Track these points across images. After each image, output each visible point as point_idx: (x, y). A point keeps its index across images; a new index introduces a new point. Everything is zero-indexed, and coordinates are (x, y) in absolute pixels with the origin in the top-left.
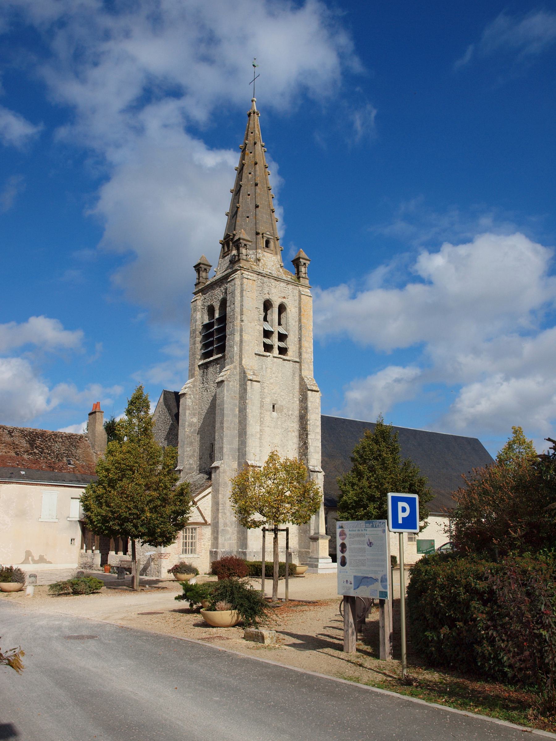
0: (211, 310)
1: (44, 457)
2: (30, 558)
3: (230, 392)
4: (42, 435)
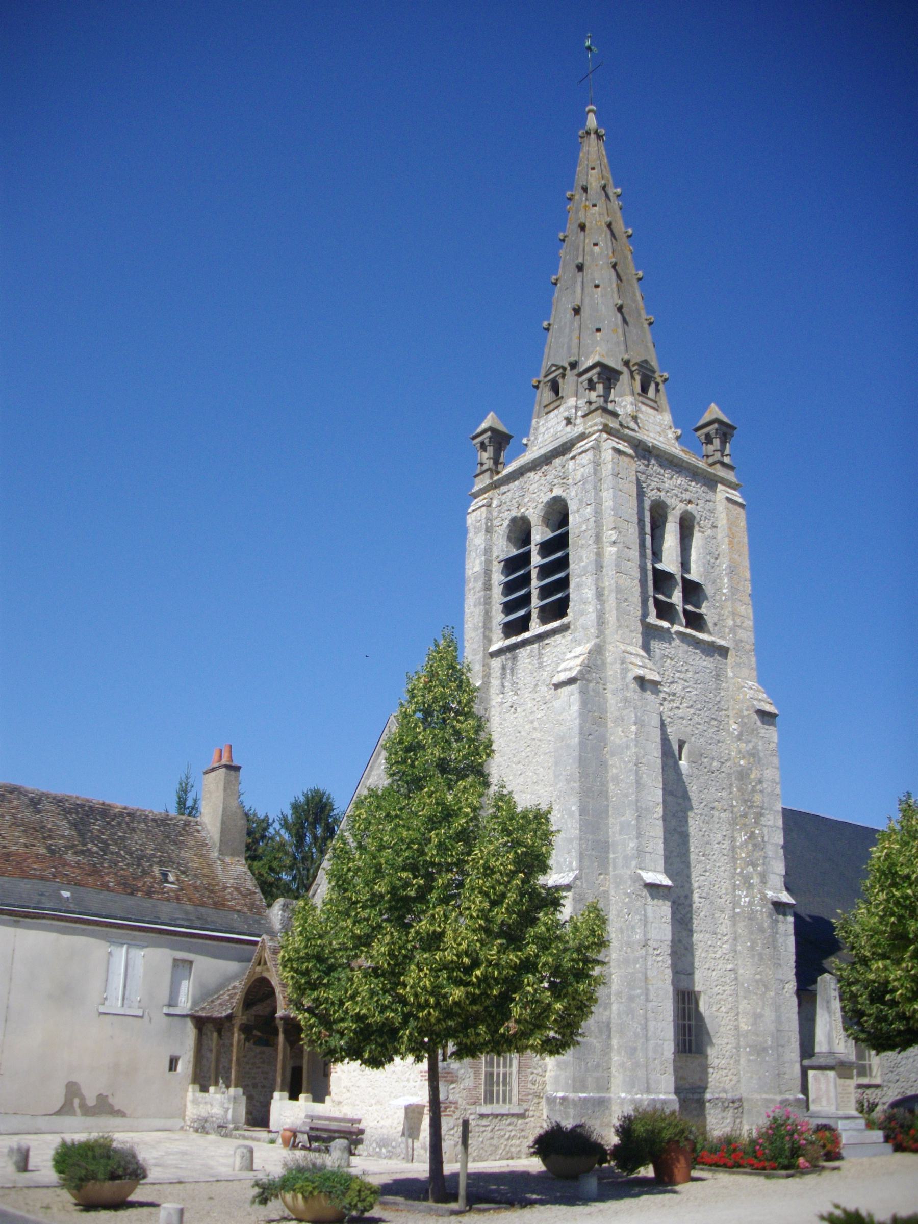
1: (111, 861)
2: (76, 1101)
4: (104, 812)
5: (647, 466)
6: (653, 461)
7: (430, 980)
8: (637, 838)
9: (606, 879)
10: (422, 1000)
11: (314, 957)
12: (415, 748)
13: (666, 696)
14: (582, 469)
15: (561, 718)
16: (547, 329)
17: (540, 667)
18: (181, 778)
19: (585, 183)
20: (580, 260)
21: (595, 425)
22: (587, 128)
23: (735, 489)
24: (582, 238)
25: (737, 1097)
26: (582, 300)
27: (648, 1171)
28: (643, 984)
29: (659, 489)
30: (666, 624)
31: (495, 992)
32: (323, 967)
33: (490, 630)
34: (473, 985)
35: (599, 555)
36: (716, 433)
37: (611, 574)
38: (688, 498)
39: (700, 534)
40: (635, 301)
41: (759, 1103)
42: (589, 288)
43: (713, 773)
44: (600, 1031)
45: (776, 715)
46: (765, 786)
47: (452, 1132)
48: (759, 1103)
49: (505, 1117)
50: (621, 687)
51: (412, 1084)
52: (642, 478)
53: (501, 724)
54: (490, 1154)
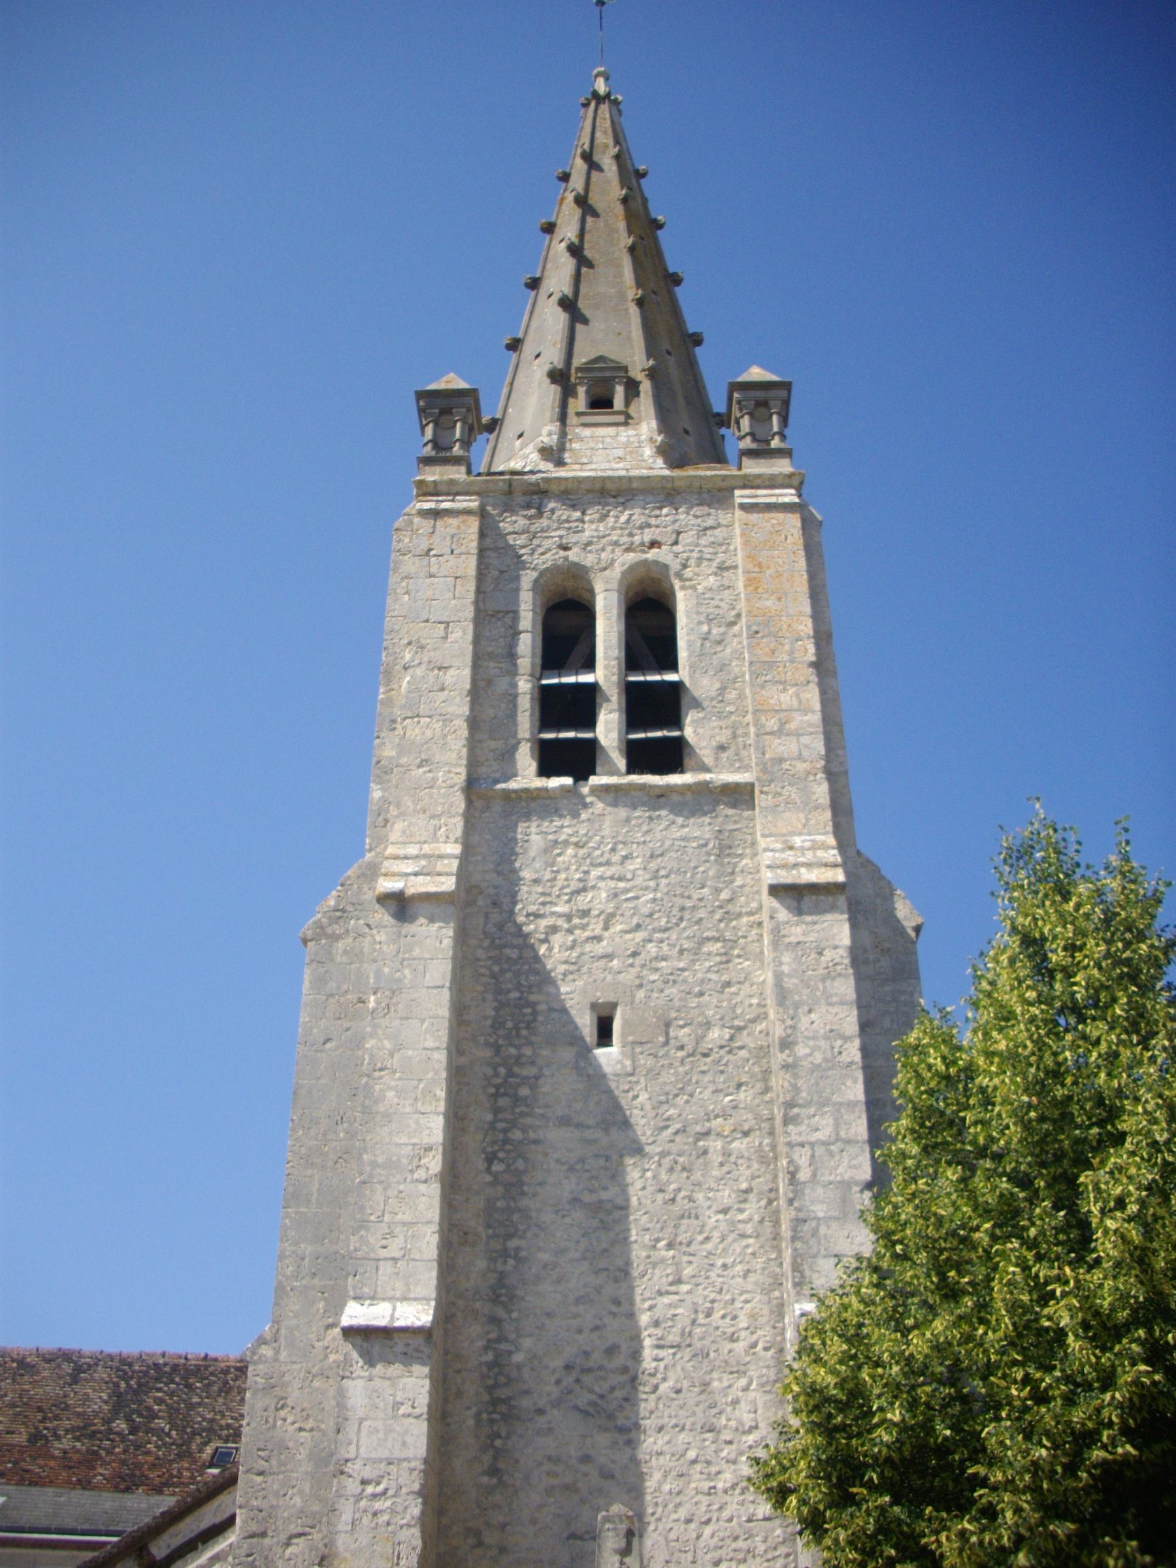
3: (332, 985)
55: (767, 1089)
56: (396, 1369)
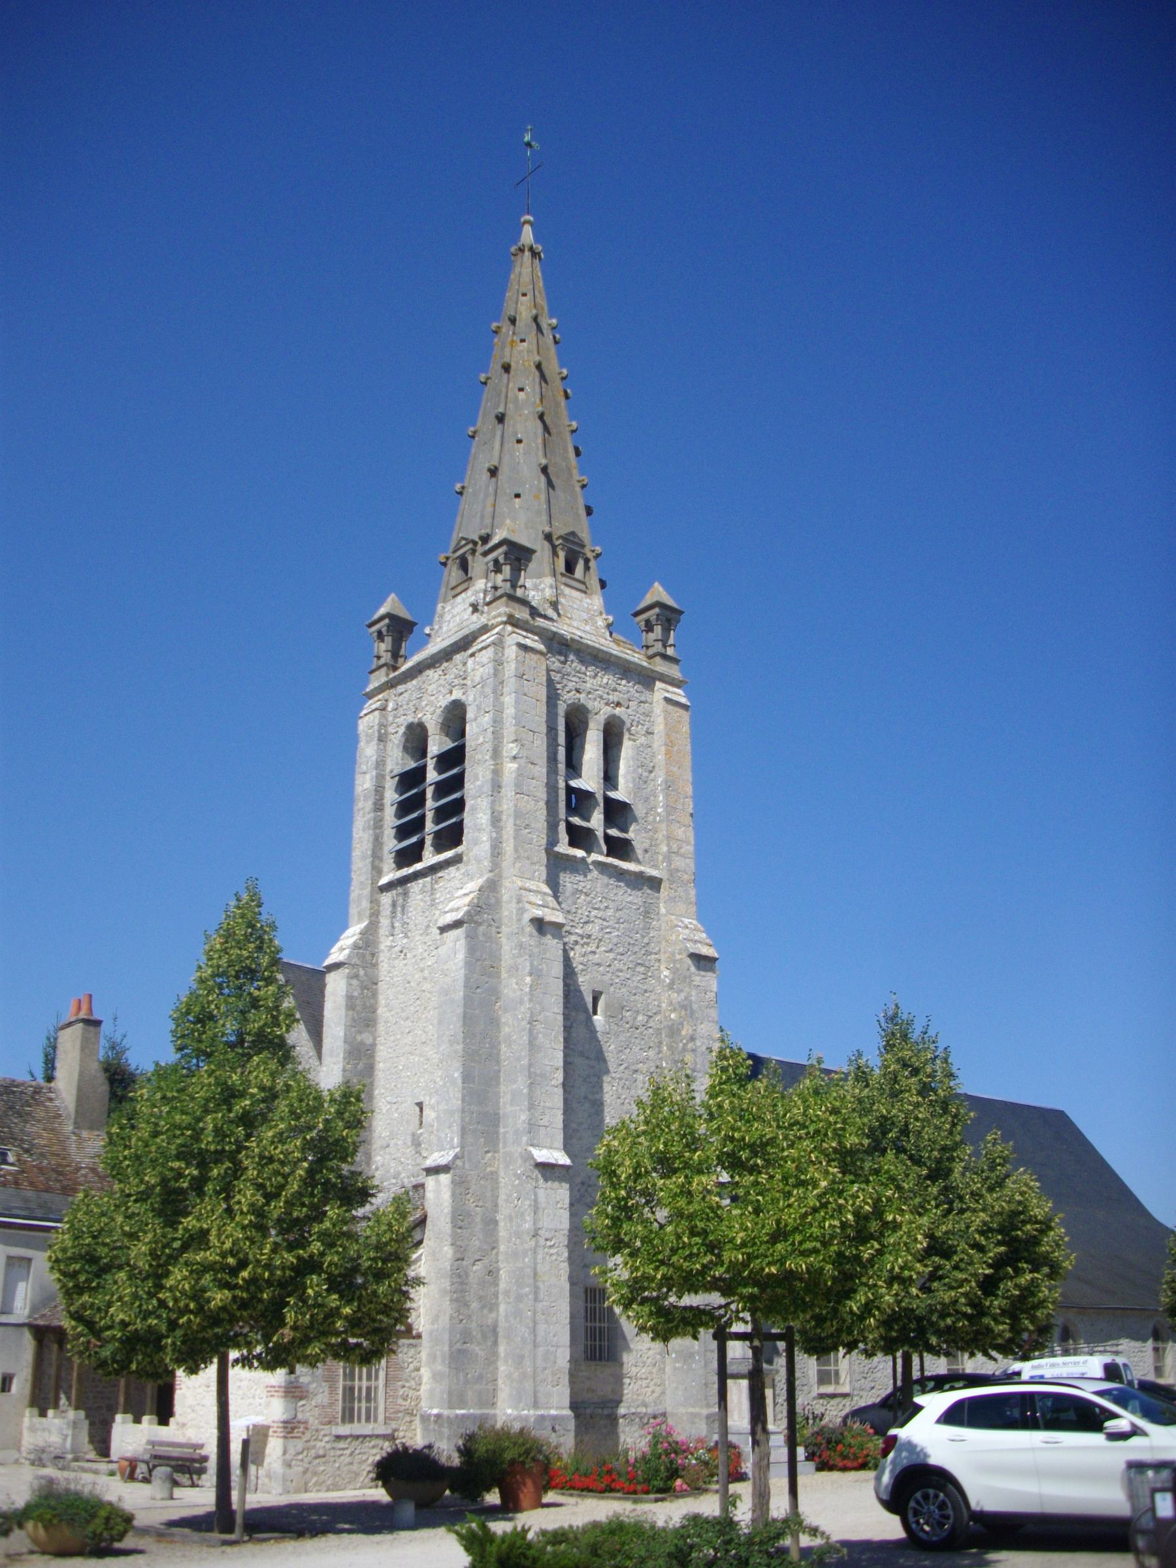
0: (416, 739)
3: (478, 953)
5: (564, 663)
6: (572, 657)
7: (189, 1283)
8: (530, 1109)
9: (494, 1157)
10: (182, 1304)
11: (82, 1257)
12: (206, 1018)
13: (579, 939)
14: (481, 669)
15: (445, 968)
16: (461, 493)
17: (432, 905)
18: (49, 1031)
19: (512, 314)
20: (501, 410)
21: (499, 615)
22: (520, 244)
23: (679, 687)
24: (505, 381)
25: (660, 1411)
26: (500, 458)
27: (493, 1498)
28: (531, 1281)
29: (578, 691)
30: (580, 853)
31: (265, 1296)
32: (94, 1268)
33: (381, 859)
34: (241, 1287)
35: (497, 772)
36: (657, 620)
37: (509, 794)
38: (616, 700)
39: (631, 742)
40: (566, 459)
41: (685, 1418)
42: (510, 444)
43: (637, 1029)
44: (484, 1337)
45: (715, 959)
46: (698, 1044)
47: (300, 1457)
48: (685, 1418)
49: (368, 1439)
50: (516, 931)
51: (258, 1401)
52: (556, 677)
53: (389, 972)
54: (349, 1482)
55: (660, 1052)
56: (556, 1184)
